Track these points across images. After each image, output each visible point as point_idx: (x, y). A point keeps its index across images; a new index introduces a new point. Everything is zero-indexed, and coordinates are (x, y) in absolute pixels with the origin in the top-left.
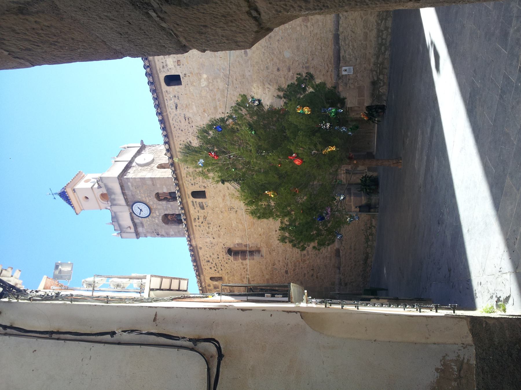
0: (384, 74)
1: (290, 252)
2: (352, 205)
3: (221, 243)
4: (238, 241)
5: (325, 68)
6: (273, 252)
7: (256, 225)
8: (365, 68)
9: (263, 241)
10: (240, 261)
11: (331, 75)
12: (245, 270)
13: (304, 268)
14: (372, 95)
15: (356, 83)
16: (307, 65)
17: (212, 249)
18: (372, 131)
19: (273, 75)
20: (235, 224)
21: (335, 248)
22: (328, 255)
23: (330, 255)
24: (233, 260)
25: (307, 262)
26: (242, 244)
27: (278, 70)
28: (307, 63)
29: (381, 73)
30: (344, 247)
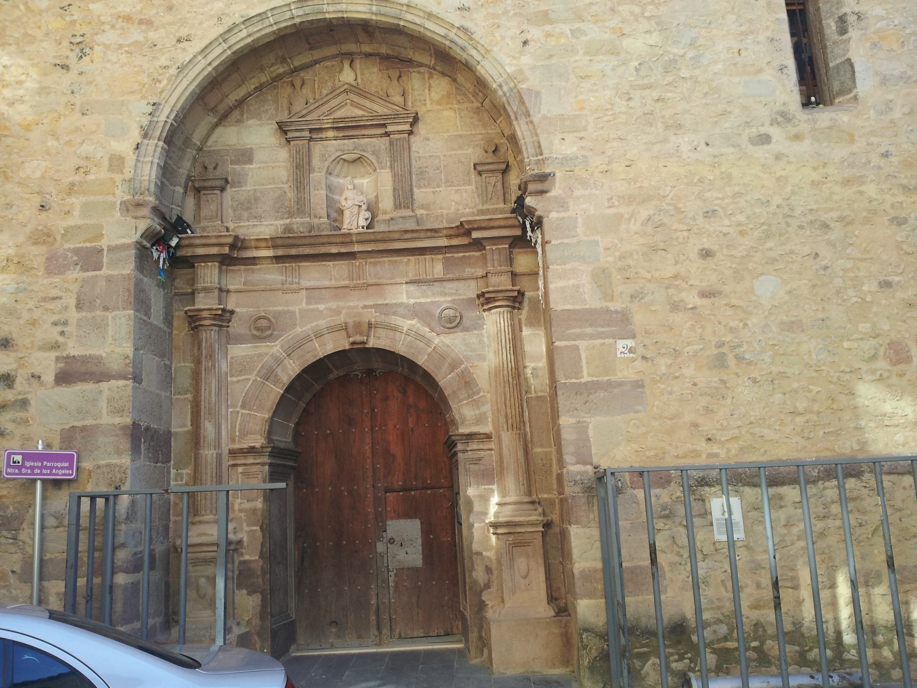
5: (723, 428)
11: (697, 454)
16: (731, 362)
18: (385, 631)
19: (685, 234)
27: (706, 254)
28: (739, 358)
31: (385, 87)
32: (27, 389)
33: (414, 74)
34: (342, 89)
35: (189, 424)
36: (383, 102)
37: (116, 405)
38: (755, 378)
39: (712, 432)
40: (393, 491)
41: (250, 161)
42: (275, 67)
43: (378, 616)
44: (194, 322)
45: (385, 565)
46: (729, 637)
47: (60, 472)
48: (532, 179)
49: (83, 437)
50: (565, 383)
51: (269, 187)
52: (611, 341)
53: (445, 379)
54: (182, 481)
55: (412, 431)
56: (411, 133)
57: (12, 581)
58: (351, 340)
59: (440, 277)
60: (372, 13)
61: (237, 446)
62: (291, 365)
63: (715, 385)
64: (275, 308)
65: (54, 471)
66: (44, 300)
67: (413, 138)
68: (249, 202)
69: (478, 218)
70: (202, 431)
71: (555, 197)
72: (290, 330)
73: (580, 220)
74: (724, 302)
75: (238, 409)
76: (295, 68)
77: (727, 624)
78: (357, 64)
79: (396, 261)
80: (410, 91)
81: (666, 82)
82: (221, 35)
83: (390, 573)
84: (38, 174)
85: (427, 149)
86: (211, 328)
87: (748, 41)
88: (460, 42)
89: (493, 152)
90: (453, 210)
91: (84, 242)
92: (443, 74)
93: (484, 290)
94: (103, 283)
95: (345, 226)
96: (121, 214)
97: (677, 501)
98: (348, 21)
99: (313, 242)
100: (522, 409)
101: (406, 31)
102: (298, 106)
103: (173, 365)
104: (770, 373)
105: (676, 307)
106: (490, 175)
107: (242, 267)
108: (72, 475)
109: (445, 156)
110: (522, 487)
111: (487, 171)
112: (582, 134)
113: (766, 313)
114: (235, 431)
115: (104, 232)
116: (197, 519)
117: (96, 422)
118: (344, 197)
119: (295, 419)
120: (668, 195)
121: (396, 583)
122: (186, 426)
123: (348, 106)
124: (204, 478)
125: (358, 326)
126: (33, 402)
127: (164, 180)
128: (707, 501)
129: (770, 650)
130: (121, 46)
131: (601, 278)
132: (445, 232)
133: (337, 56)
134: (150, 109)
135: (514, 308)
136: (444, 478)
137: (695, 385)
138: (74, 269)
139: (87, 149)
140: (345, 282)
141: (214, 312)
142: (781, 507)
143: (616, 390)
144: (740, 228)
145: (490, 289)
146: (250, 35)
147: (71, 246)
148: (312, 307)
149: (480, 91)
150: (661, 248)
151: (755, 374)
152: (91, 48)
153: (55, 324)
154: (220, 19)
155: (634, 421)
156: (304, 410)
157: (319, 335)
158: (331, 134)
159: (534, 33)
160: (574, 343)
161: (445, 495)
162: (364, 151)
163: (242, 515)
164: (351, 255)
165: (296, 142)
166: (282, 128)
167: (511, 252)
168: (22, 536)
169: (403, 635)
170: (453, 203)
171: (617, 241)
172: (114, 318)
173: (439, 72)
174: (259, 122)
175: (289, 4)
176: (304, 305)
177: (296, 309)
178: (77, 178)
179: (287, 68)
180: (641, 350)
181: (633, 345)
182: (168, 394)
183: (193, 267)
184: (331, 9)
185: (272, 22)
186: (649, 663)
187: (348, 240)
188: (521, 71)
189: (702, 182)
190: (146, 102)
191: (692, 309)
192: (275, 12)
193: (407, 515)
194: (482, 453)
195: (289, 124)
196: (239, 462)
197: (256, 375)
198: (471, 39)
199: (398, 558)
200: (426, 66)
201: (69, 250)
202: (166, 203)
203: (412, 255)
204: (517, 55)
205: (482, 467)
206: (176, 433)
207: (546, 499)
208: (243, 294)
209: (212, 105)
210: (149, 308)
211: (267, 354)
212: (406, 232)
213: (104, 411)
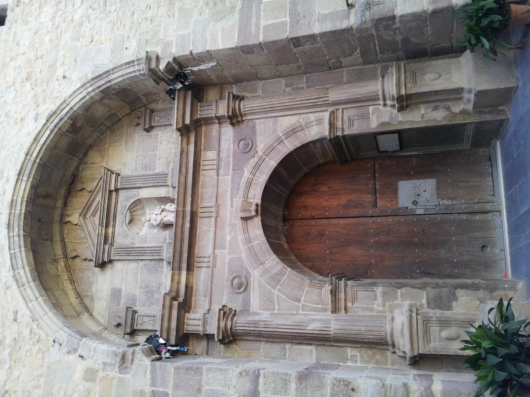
18: (489, 207)
33: (83, 174)
34: (82, 221)
37: (280, 386)
41: (120, 291)
43: (476, 213)
45: (434, 207)
48: (148, 65)
51: (139, 277)
52: (262, 5)
54: (357, 356)
59: (216, 153)
61: (330, 307)
64: (226, 273)
67: (123, 174)
71: (162, 50)
72: (243, 262)
73: (179, 33)
75: (300, 305)
76: (63, 254)
82: (19, 287)
85: (131, 164)
86: (234, 322)
88: (57, 120)
90: (172, 145)
96: (128, 373)
98: (30, 199)
99: (180, 239)
101: (45, 160)
106: (153, 120)
107: (193, 298)
109: (137, 152)
111: (150, 122)
114: (318, 308)
115: (140, 389)
121: (449, 199)
122: (312, 351)
124: (354, 332)
125: (244, 210)
131: (218, 17)
132: (185, 145)
134: (57, 345)
136: (367, 164)
140: (213, 220)
141: (222, 317)
146: (24, 267)
149: (99, 127)
157: (249, 240)
158: (110, 230)
160: (261, 29)
161: (380, 163)
162: (126, 207)
166: (102, 265)
169: (492, 193)
170: (168, 146)
171: (196, 9)
172: (208, 384)
174: (95, 283)
175: (9, 237)
176: (226, 251)
177: (228, 257)
179: (62, 260)
183: (187, 334)
184: (18, 208)
185: (17, 250)
187: (181, 213)
190: (51, 348)
192: (12, 247)
193: (395, 191)
194: (346, 118)
195: (98, 258)
196: (343, 305)
197: (275, 289)
199: (429, 197)
206: (317, 359)
208: (213, 299)
211: (259, 280)
212: (180, 171)
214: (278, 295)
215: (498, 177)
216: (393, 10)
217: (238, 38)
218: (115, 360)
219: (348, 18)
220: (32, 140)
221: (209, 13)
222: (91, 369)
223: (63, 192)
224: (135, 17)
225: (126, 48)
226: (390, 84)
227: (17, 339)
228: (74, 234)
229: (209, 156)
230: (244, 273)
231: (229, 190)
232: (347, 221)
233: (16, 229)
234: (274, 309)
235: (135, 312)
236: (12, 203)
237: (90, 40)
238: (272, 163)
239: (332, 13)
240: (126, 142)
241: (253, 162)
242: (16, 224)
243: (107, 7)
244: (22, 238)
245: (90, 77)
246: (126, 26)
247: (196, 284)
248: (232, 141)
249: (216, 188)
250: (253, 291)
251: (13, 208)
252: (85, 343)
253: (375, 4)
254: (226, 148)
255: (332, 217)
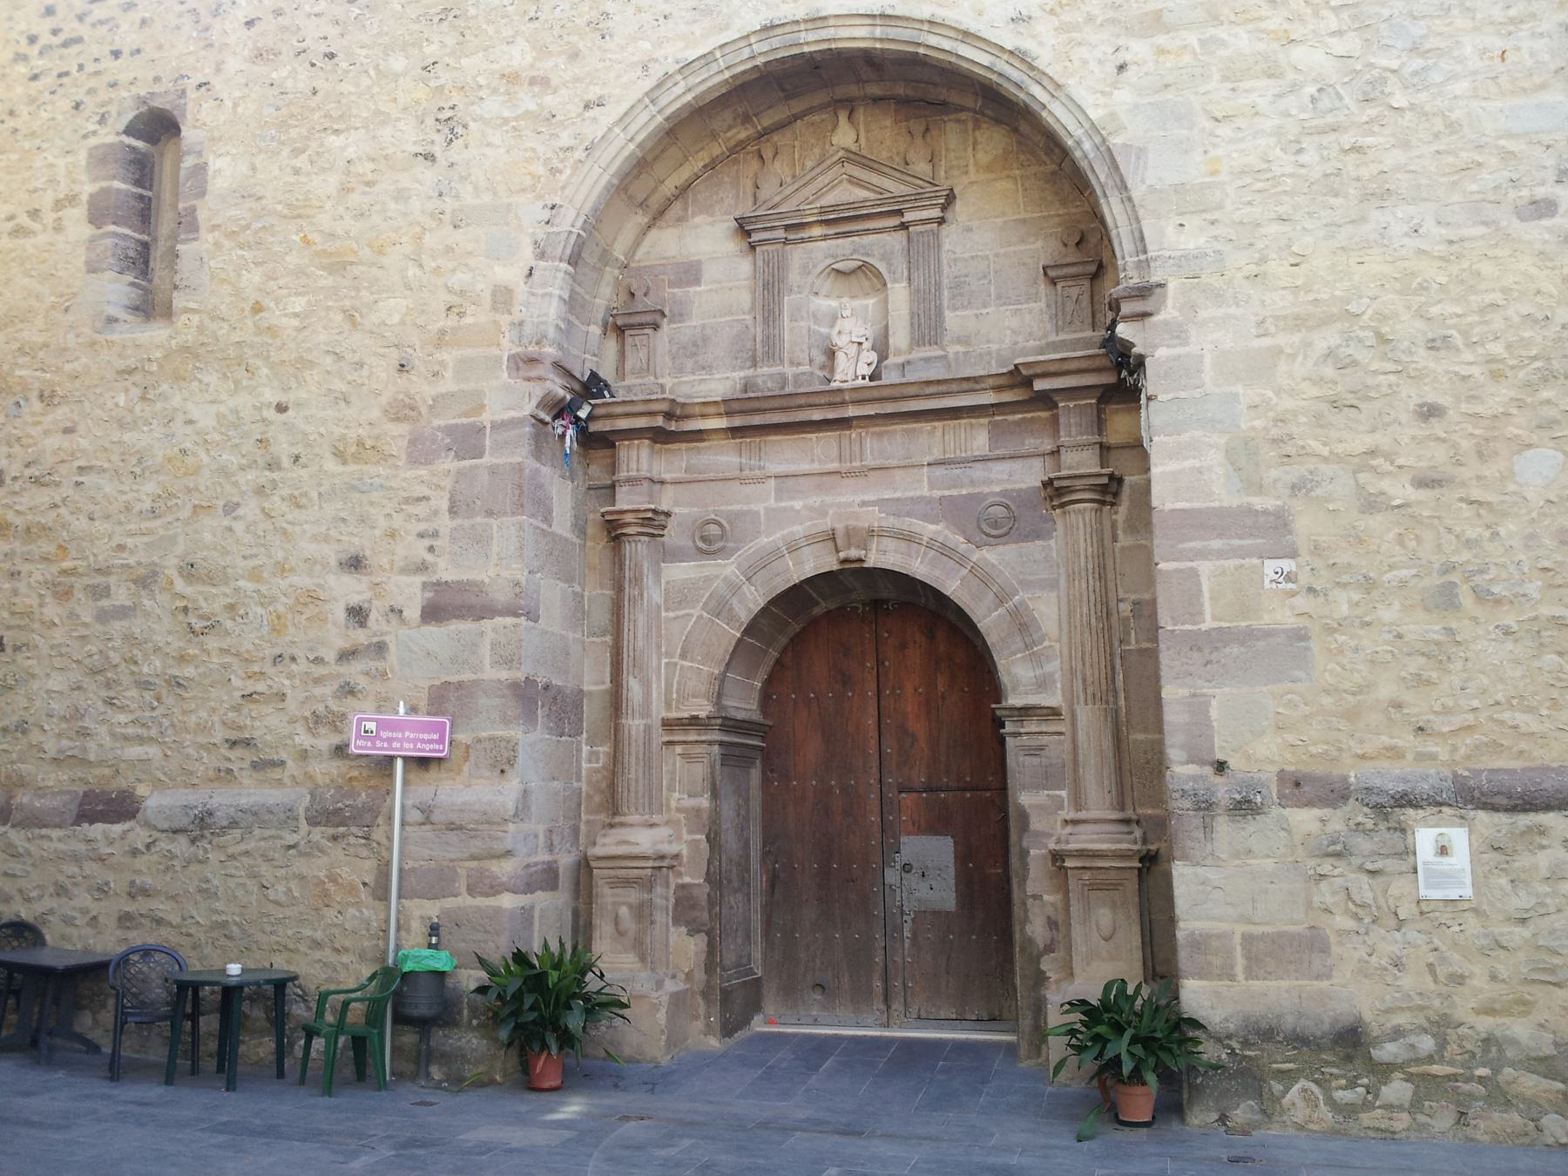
0: (1415, 1106)
1: (130, 496)
2: (449, 903)
3: (218, 70)
4: (219, 171)
5: (1446, 711)
6: (136, 392)
7: (327, 281)
8: (1459, 979)
9: (213, 326)
10: (88, 189)
11: (1395, 753)
12: (24, 220)
13: (15, 593)
14: (1264, 1033)
15: (1350, 924)
16: (1466, 599)
17: (180, 16)
18: (897, 1006)
19: (1393, 378)
20: (343, 149)
21: (141, 790)
22: (91, 745)
23: (92, 757)
24: (93, 141)
25: (52, 611)
26: (202, 193)
27: (1430, 412)
28: (1481, 595)
29: (1428, 1087)
30: (148, 846)
31: (902, 150)
32: (385, 628)
33: (950, 125)
34: (836, 158)
35: (608, 680)
36: (898, 175)
38: (1509, 627)
39: (1425, 718)
40: (910, 790)
41: (697, 281)
42: (735, 130)
43: (886, 981)
44: (615, 529)
46: (1436, 1057)
47: (428, 747)
48: (1126, 294)
49: (459, 698)
50: (1173, 631)
51: (723, 320)
52: (1256, 561)
53: (988, 620)
55: (943, 698)
56: (941, 221)
57: (363, 897)
58: (842, 555)
60: (875, 39)
61: (674, 715)
62: (752, 594)
63: (1436, 637)
64: (730, 508)
65: (419, 745)
66: (407, 501)
68: (695, 345)
69: (1042, 358)
70: (624, 692)
71: (1166, 323)
73: (1208, 360)
74: (1457, 496)
76: (764, 129)
77: (1434, 1036)
78: (860, 115)
79: (914, 430)
80: (943, 152)
81: (1365, 119)
82: (647, 94)
83: (905, 918)
84: (396, 319)
86: (637, 538)
87: (1521, 34)
89: (1077, 244)
91: (460, 416)
92: (997, 121)
93: (1052, 475)
94: (485, 477)
95: (838, 377)
97: (1356, 831)
99: (785, 405)
100: (1113, 669)
101: (929, 61)
102: (768, 191)
103: (586, 593)
104: (1536, 618)
105: (1372, 504)
106: (1071, 283)
107: (684, 446)
108: (443, 751)
109: (997, 255)
110: (1108, 797)
111: (1065, 277)
112: (1216, 215)
113: (1534, 515)
116: (618, 819)
117: (474, 677)
118: (837, 329)
119: (762, 674)
120: (1363, 313)
122: (603, 683)
123: (845, 184)
124: (626, 760)
125: (849, 533)
126: (392, 647)
127: (572, 318)
128: (1409, 832)
129: (1508, 1083)
130: (506, 121)
131: (1242, 455)
132: (991, 382)
133: (829, 104)
134: (547, 214)
135: (1103, 503)
137: (1400, 636)
138: (447, 457)
139: (460, 279)
140: (834, 466)
142: (1543, 847)
143: (1261, 644)
144: (1494, 366)
145: (1064, 473)
146: (689, 90)
147: (442, 423)
148: (783, 504)
150: (1349, 403)
151: (1510, 620)
152: (465, 127)
153: (421, 535)
154: (645, 68)
155: (1289, 696)
156: (778, 661)
157: (793, 548)
158: (817, 231)
159: (1138, 49)
160: (1190, 564)
161: (993, 801)
162: (868, 255)
163: (682, 816)
164: (843, 423)
165: (764, 248)
166: (744, 229)
167: (1100, 412)
168: (378, 834)
169: (923, 1015)
170: (1008, 332)
171: (1270, 394)
173: (990, 118)
174: (711, 219)
175: (748, 36)
176: (772, 501)
177: (759, 507)
178: (452, 321)
180: (1305, 579)
181: (1294, 569)
182: (579, 636)
183: (613, 446)
184: (811, 37)
185: (723, 65)
186: (1297, 1087)
187: (838, 399)
188: (1112, 116)
189: (1426, 289)
190: (541, 204)
191: (1398, 507)
192: (727, 50)
194: (1045, 739)
196: (676, 738)
198: (1032, 68)
200: (968, 110)
201: (439, 428)
202: (575, 352)
203: (939, 420)
204: (1108, 89)
205: (1044, 760)
206: (590, 693)
207: (1150, 817)
209: (640, 197)
210: (550, 511)
212: (929, 383)
213: (487, 662)
214: (692, 615)
215: (954, 1029)
216: (1185, 857)
217: (1173, 511)
218: (530, 343)
219: (1190, 761)
220: (963, 27)
221: (1253, 429)
222: (511, 298)
223: (900, 90)
224: (1274, 228)
225: (1181, 225)
226: (1095, 836)
227: (554, 121)
228: (813, 141)
229: (978, 438)
230: (730, 545)
231: (897, 495)
232: (873, 733)
233: (764, 47)
234: (667, 610)
235: (656, 327)
236: (817, 20)
237: (1219, 115)
238: (952, 586)
239: (1209, 726)
240: (1024, 221)
241: (958, 540)
242: (776, 43)
243: (1316, 138)
244: (749, 66)
245: (1116, 141)
246: (1249, 209)
247: (709, 448)
248: (1009, 487)
249: (901, 463)
250: (698, 566)
251: (810, 26)
252: (557, 270)
253: (1208, 820)
254: (993, 476)
255: (882, 702)
